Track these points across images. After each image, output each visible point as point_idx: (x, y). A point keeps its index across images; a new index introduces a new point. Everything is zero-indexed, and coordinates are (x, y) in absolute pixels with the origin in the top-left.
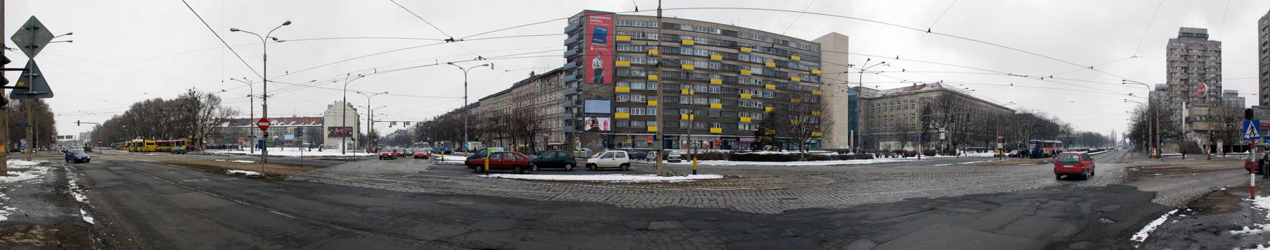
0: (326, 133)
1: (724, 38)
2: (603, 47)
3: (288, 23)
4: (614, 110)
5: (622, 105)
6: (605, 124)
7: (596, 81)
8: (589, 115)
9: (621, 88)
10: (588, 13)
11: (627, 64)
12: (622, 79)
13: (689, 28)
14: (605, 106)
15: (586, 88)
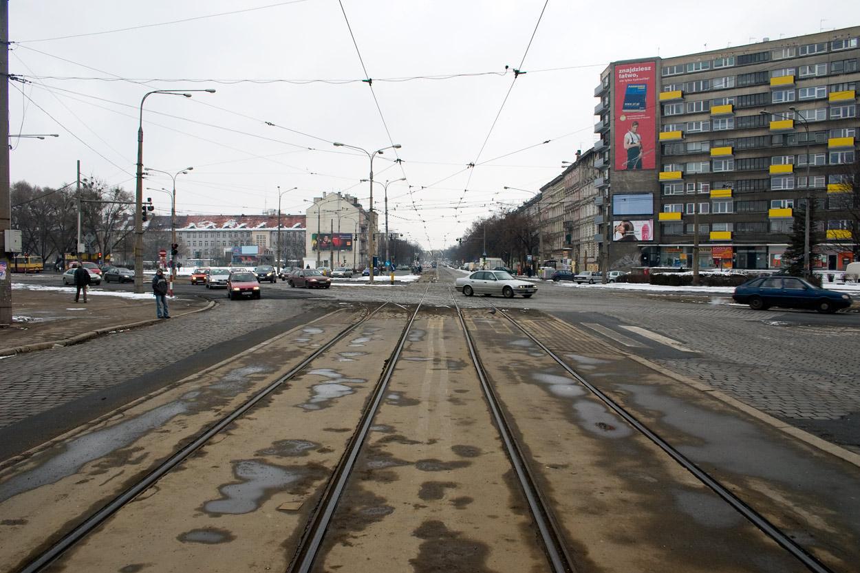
0: (310, 243)
1: (826, 395)
2: (640, 114)
3: (506, 188)
4: (659, 206)
5: (673, 199)
6: (645, 230)
7: (630, 167)
8: (619, 217)
9: (671, 174)
10: (616, 67)
11: (677, 135)
12: (673, 158)
13: (786, 54)
14: (645, 204)
15: (616, 177)
